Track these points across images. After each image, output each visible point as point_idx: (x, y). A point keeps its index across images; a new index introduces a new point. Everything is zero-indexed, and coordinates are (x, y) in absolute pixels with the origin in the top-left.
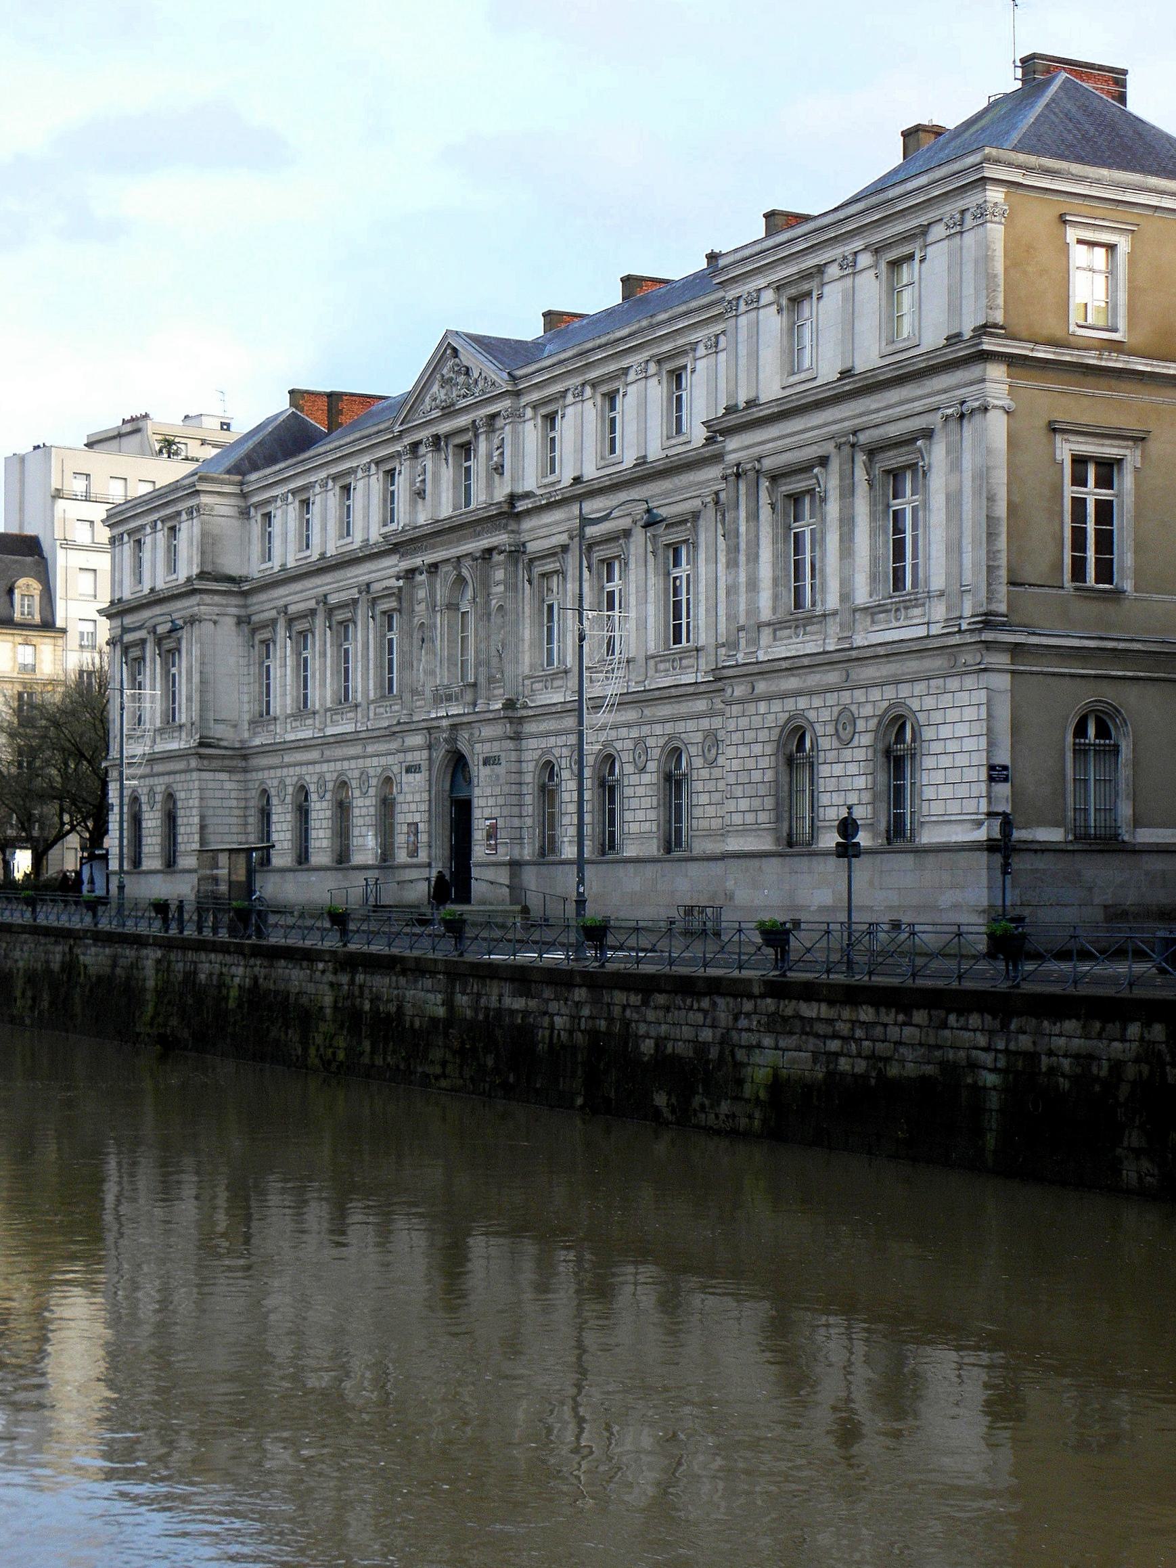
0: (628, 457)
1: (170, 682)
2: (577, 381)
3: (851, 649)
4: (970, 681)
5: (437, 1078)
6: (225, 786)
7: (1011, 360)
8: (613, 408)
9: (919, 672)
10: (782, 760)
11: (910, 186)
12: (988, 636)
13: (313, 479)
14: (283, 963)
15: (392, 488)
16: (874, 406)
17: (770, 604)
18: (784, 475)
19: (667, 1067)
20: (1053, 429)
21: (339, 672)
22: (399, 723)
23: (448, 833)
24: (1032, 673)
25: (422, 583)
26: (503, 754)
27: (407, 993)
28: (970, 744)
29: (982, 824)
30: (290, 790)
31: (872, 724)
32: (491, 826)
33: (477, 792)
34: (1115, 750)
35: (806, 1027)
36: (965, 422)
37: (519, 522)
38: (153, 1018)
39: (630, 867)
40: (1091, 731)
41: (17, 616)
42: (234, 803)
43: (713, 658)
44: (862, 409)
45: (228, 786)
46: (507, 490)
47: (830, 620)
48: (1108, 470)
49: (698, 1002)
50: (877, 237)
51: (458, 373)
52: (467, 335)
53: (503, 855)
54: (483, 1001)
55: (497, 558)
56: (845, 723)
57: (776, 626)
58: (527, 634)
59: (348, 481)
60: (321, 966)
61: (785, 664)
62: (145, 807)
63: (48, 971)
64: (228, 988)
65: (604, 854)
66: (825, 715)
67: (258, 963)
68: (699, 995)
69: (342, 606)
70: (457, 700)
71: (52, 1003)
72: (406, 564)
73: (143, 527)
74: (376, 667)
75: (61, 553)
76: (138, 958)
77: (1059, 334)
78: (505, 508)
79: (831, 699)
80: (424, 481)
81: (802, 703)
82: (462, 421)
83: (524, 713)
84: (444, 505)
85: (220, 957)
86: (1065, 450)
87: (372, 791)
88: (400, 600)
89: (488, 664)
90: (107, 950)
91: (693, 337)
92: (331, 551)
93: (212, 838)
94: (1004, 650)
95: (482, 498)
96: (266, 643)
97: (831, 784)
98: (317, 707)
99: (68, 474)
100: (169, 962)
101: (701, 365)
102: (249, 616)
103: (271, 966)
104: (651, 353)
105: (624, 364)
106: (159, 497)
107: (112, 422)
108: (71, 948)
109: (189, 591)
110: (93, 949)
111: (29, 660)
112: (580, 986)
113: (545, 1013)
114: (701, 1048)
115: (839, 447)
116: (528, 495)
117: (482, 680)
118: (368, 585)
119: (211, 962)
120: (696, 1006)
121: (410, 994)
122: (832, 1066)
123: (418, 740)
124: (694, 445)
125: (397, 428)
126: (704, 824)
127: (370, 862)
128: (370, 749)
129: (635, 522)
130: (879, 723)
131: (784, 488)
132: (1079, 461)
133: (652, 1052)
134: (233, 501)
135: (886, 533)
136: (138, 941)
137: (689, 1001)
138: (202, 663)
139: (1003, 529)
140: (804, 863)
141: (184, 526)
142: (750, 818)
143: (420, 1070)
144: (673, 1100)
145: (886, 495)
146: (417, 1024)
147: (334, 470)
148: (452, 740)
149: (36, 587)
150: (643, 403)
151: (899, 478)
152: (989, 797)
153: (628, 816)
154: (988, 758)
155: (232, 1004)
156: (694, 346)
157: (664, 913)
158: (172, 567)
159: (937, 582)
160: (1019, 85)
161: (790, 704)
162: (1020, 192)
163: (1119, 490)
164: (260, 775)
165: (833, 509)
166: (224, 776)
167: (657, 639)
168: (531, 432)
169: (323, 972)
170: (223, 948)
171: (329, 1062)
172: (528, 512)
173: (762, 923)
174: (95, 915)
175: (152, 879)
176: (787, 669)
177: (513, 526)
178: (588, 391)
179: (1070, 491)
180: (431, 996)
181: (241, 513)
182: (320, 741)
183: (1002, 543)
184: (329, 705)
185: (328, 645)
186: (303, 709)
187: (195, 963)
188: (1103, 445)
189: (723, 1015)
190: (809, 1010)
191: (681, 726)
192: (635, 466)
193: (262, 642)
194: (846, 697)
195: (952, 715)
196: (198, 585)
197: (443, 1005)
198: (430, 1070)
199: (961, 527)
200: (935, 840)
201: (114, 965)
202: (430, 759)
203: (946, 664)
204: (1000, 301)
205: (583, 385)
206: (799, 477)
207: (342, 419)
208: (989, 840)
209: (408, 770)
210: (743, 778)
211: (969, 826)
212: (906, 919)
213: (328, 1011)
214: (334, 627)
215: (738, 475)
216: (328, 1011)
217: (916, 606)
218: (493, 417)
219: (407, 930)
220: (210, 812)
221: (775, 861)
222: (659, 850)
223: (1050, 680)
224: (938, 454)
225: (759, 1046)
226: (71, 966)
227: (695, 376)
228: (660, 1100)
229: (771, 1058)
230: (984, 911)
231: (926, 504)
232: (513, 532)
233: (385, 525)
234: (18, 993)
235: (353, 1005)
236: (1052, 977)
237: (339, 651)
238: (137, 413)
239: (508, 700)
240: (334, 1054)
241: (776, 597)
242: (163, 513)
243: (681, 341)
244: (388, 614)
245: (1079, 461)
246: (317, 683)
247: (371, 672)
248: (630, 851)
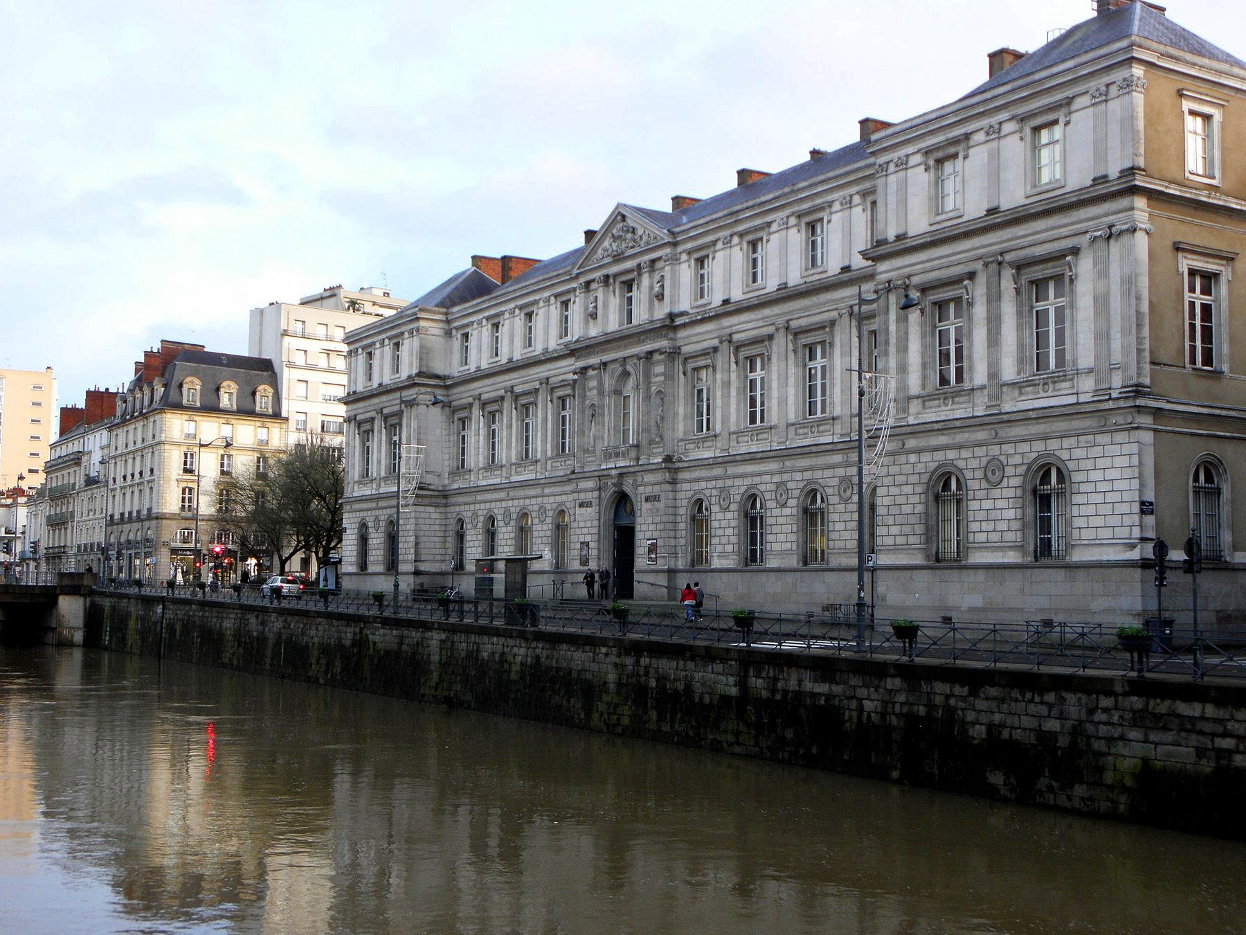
0: (503, 359)
1: (394, 446)
2: (727, 233)
3: (1000, 414)
4: (1120, 437)
5: (730, 744)
6: (432, 515)
7: (1151, 195)
8: (754, 251)
10: (931, 498)
11: (1055, 70)
16: (1021, 233)
17: (919, 382)
18: (932, 288)
19: (999, 748)
20: (1177, 248)
22: (573, 472)
24: (1167, 432)
25: (592, 377)
26: (662, 494)
27: (696, 675)
33: (639, 520)
34: (1218, 492)
35: (1187, 725)
36: (1112, 241)
39: (773, 575)
41: (258, 409)
42: (438, 528)
44: (1009, 236)
45: (434, 516)
46: (667, 310)
47: (978, 393)
48: (1209, 280)
49: (1041, 696)
50: (1022, 109)
53: (662, 564)
55: (657, 357)
56: (994, 472)
57: (925, 398)
58: (681, 410)
60: (604, 650)
62: (371, 530)
63: (340, 646)
65: (747, 565)
66: (975, 463)
68: (1042, 690)
69: (525, 394)
71: (343, 670)
72: (581, 364)
75: (286, 370)
77: (1179, 178)
78: (668, 322)
79: (980, 451)
80: (596, 307)
81: (951, 455)
82: (629, 264)
83: (680, 465)
85: (502, 640)
86: (1186, 263)
87: (549, 520)
88: (574, 389)
89: (649, 431)
91: (829, 198)
92: (484, 366)
93: (422, 551)
98: (539, 456)
99: (292, 322)
100: (453, 643)
103: (554, 648)
105: (769, 218)
106: (388, 323)
107: (317, 290)
108: (361, 629)
109: (411, 384)
111: (264, 437)
112: (893, 676)
113: (853, 697)
114: (1046, 738)
115: (986, 265)
116: (682, 314)
120: (1037, 699)
121: (698, 676)
122: (1224, 762)
123: (590, 484)
124: (830, 273)
125: (575, 271)
126: (839, 544)
128: (547, 491)
129: (777, 330)
130: (1028, 469)
132: (1192, 273)
134: (441, 325)
135: (1031, 328)
136: (425, 626)
137: (1028, 695)
138: (419, 433)
139: (1147, 321)
144: (1013, 780)
145: (1030, 299)
146: (707, 700)
147: (520, 302)
148: (619, 485)
149: (270, 391)
153: (770, 538)
155: (514, 676)
156: (830, 204)
157: (803, 609)
158: (396, 369)
159: (1086, 359)
164: (457, 509)
165: (980, 311)
166: (432, 509)
168: (686, 272)
169: (607, 655)
171: (614, 726)
172: (684, 325)
173: (1122, 629)
175: (375, 578)
177: (671, 335)
178: (736, 240)
179: (1187, 294)
183: (1146, 331)
186: (492, 464)
190: (1183, 708)
191: (818, 474)
194: (995, 450)
196: (417, 380)
198: (723, 738)
199: (1108, 320)
201: (401, 643)
203: (1095, 424)
204: (1142, 150)
205: (731, 236)
207: (512, 274)
210: (894, 510)
211: (1121, 548)
212: (1058, 618)
213: (612, 686)
215: (889, 291)
216: (612, 686)
218: (653, 261)
219: (598, 618)
220: (422, 534)
223: (1177, 436)
224: (1085, 266)
225: (1122, 738)
226: (361, 643)
228: (996, 779)
229: (1130, 752)
230: (1139, 615)
231: (1072, 305)
234: (313, 661)
235: (639, 682)
236: (1178, 669)
240: (619, 719)
241: (924, 378)
242: (389, 334)
243: (818, 201)
244: (563, 399)
245: (1192, 273)
248: (772, 563)
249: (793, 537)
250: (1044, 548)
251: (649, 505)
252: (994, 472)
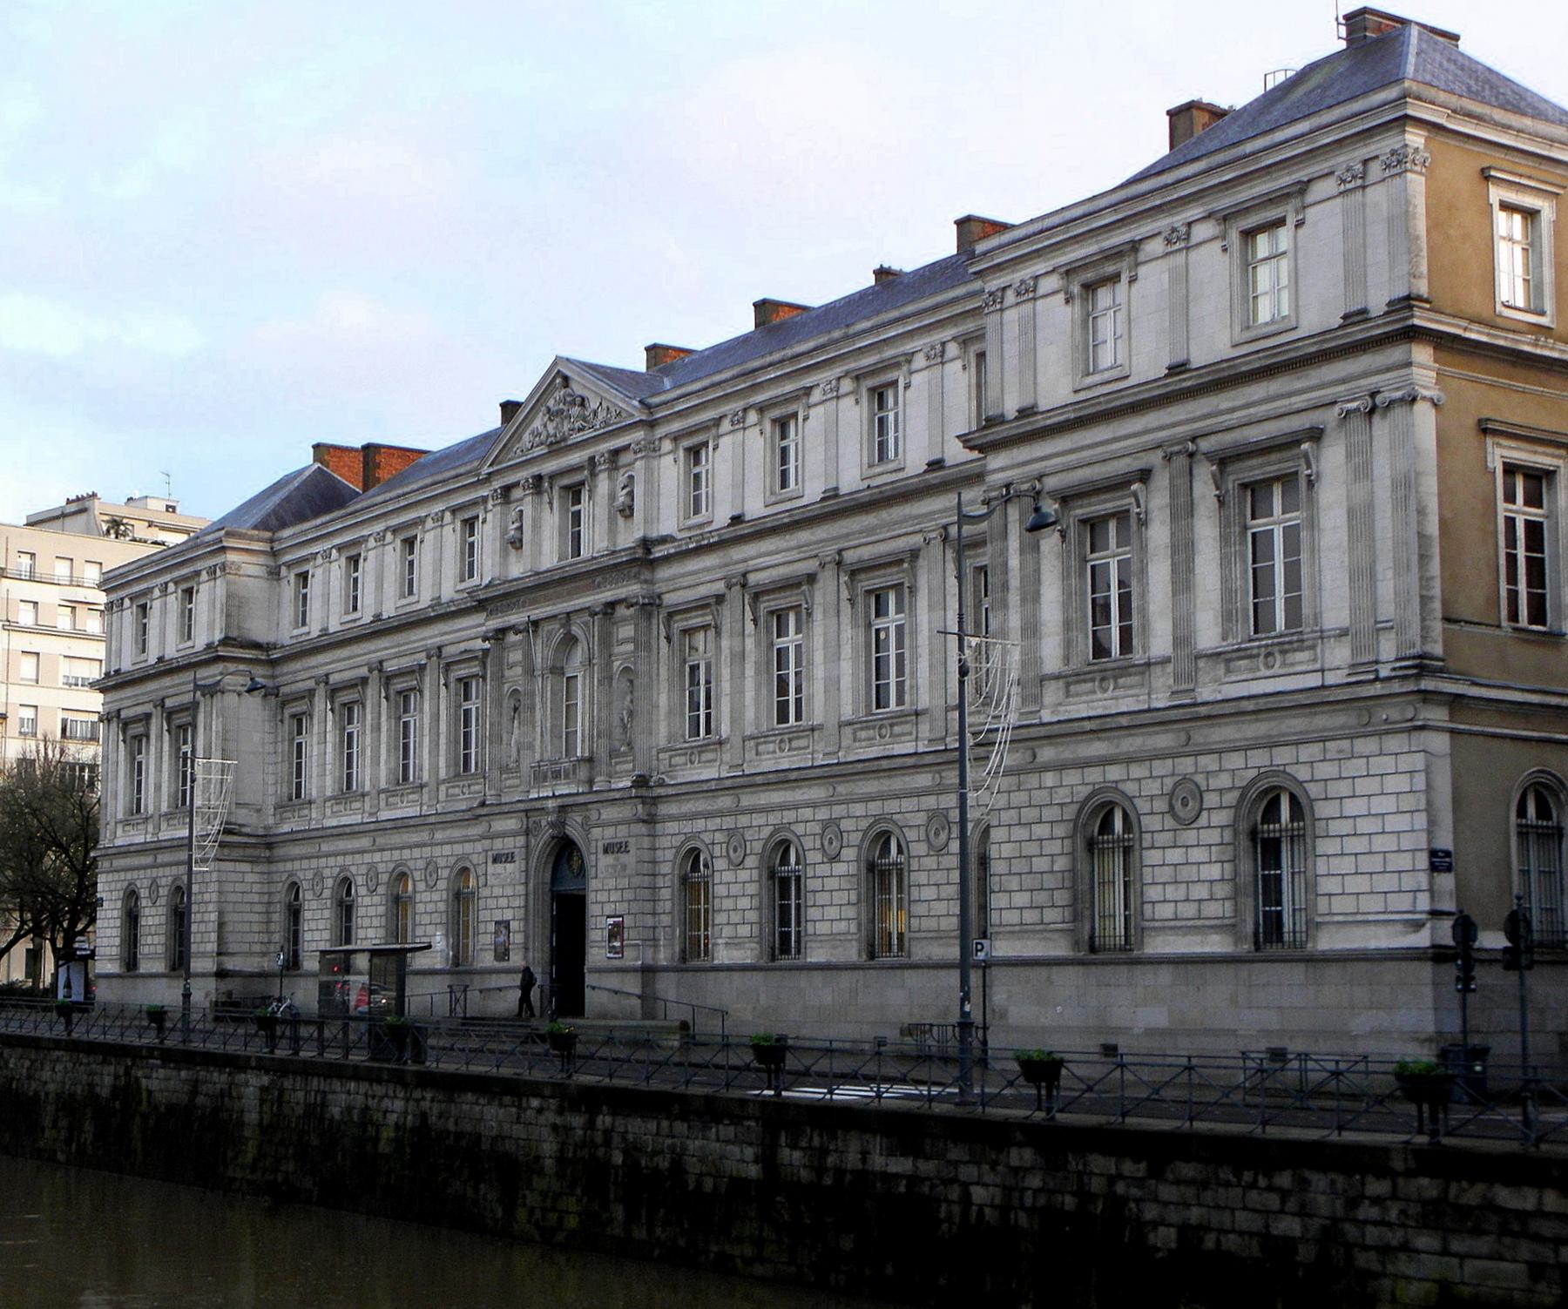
1: (183, 761)
2: (737, 405)
4: (1394, 743)
6: (247, 876)
9: (1307, 732)
11: (1279, 136)
12: (1427, 684)
13: (366, 532)
14: (470, 1096)
15: (696, 470)
16: (1225, 405)
20: (1485, 429)
21: (397, 748)
22: (483, 804)
23: (548, 932)
26: (632, 841)
28: (1402, 822)
29: (1423, 925)
30: (329, 883)
31: (1231, 798)
32: (615, 925)
33: (594, 884)
35: (1515, 1225)
36: (1376, 418)
37: (653, 570)
38: (255, 1161)
39: (817, 976)
40: (1531, 810)
42: (256, 898)
43: (941, 724)
45: (250, 878)
46: (639, 534)
48: (1538, 482)
50: (1225, 202)
51: (573, 403)
52: (584, 364)
53: (632, 958)
54: (831, 1160)
55: (622, 611)
57: (1070, 680)
58: (663, 700)
59: (305, 568)
60: (535, 1103)
61: (1088, 725)
62: (144, 902)
64: (378, 1127)
67: (429, 1095)
70: (567, 777)
72: (495, 623)
73: (150, 590)
74: (448, 742)
76: (231, 1084)
77: (1486, 314)
78: (640, 553)
79: (1162, 767)
80: (520, 528)
81: (1114, 773)
84: (547, 551)
85: (364, 1087)
86: (1499, 454)
90: (183, 1074)
91: (909, 347)
93: (230, 938)
94: (1440, 704)
95: (605, 544)
96: (298, 718)
97: (1165, 874)
99: (13, 553)
100: (282, 1091)
101: (917, 379)
102: (278, 688)
103: (451, 1100)
104: (846, 368)
105: (807, 381)
106: (174, 555)
108: (127, 1073)
109: (212, 657)
110: (161, 1071)
113: (955, 1180)
115: (1168, 458)
116: (664, 540)
117: (602, 754)
118: (440, 648)
119: (349, 1093)
120: (1262, 1182)
121: (694, 1145)
123: (512, 824)
125: (486, 470)
126: (928, 924)
127: (438, 966)
128: (439, 836)
130: (1242, 797)
131: (1079, 511)
132: (1510, 470)
133: (1173, 1245)
134: (262, 560)
135: (1245, 562)
137: (1248, 1176)
138: (225, 740)
141: (204, 588)
142: (1030, 916)
143: (714, 1248)
146: (708, 1184)
147: (395, 521)
148: (560, 824)
150: (833, 429)
151: (1098, 530)
152: (1431, 891)
154: (1429, 841)
157: (869, 1032)
158: (187, 633)
160: (1343, 45)
161: (1094, 775)
162: (1440, 138)
163: (1550, 511)
164: (289, 866)
165: (1159, 533)
166: (246, 867)
167: (855, 702)
169: (540, 1111)
170: (357, 1074)
172: (667, 559)
174: (68, 1023)
175: (152, 983)
176: (1092, 731)
177: (646, 575)
178: (752, 417)
179: (1502, 507)
180: (734, 1150)
181: (270, 573)
182: (372, 826)
183: (1435, 567)
184: (383, 785)
185: (384, 718)
186: (347, 790)
187: (324, 1092)
188: (1535, 453)
189: (1321, 1199)
192: (823, 499)
193: (293, 716)
194: (1186, 765)
195: (1363, 786)
197: (756, 1162)
200: (1339, 946)
201: (194, 1092)
202: (527, 847)
204: (1424, 268)
205: (745, 410)
206: (1103, 497)
207: (380, 474)
208: (1434, 946)
209: (496, 860)
210: (1019, 866)
212: (1295, 1046)
213: (549, 1163)
214: (392, 697)
215: (1007, 500)
216: (549, 1163)
217: (1301, 649)
220: (230, 908)
221: (1071, 971)
222: (860, 955)
223: (1496, 743)
224: (1332, 459)
225: (1405, 1247)
226: (127, 1091)
227: (908, 393)
230: (1429, 1040)
231: (1313, 523)
232: (646, 582)
233: (462, 580)
234: (47, 1122)
237: (397, 725)
238: (83, 492)
239: (639, 776)
240: (561, 1219)
241: (1068, 644)
242: (176, 574)
243: (889, 353)
244: (465, 682)
245: (1510, 470)
246: (368, 761)
247: (443, 748)
248: (816, 955)
249: (850, 912)
250: (1271, 929)
252: (1185, 803)
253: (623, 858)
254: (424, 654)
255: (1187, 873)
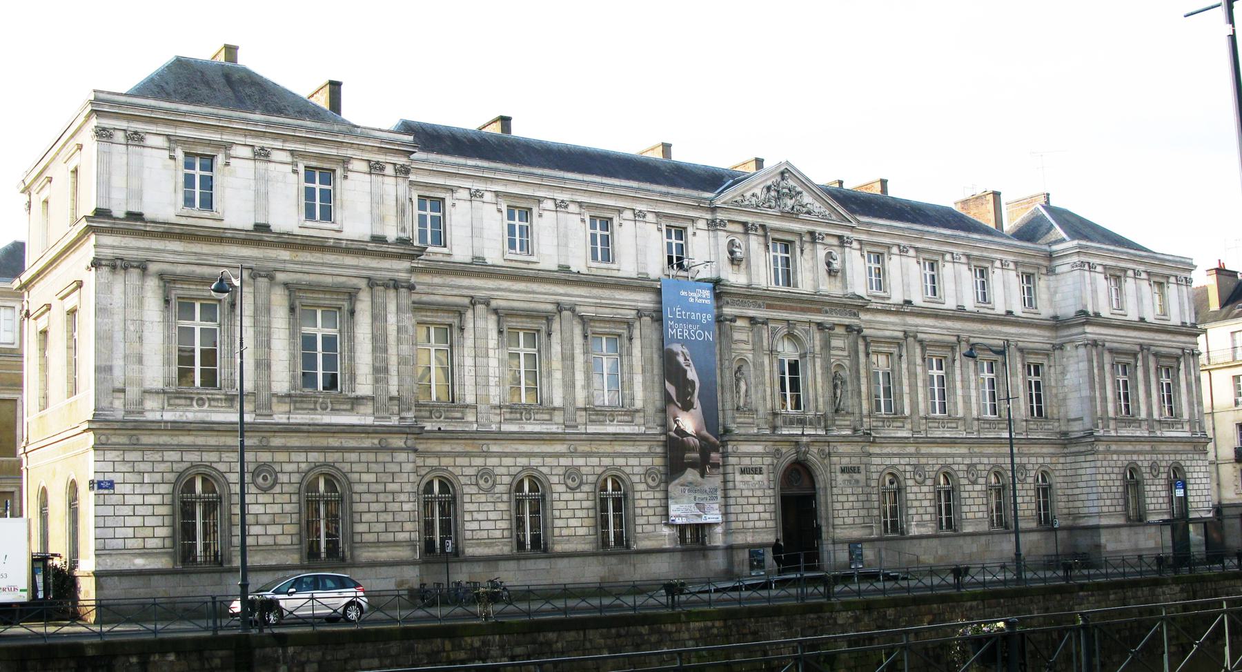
39: (969, 539)
66: (1146, 464)
97: (1151, 494)
140: (1140, 530)
142: (1112, 509)
153: (1033, 506)
195: (1197, 469)
210: (1107, 489)
248: (968, 529)
250: (949, 524)
251: (846, 476)
253: (856, 476)
254: (634, 312)
255: (1157, 494)
